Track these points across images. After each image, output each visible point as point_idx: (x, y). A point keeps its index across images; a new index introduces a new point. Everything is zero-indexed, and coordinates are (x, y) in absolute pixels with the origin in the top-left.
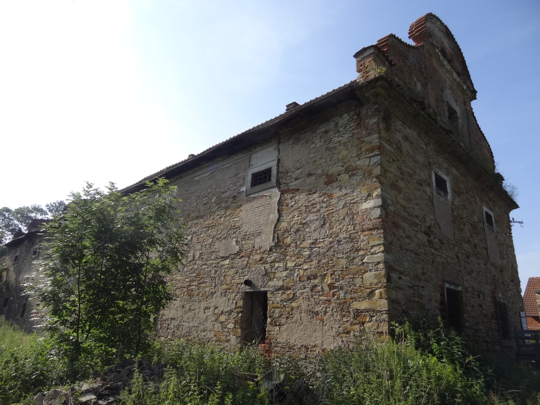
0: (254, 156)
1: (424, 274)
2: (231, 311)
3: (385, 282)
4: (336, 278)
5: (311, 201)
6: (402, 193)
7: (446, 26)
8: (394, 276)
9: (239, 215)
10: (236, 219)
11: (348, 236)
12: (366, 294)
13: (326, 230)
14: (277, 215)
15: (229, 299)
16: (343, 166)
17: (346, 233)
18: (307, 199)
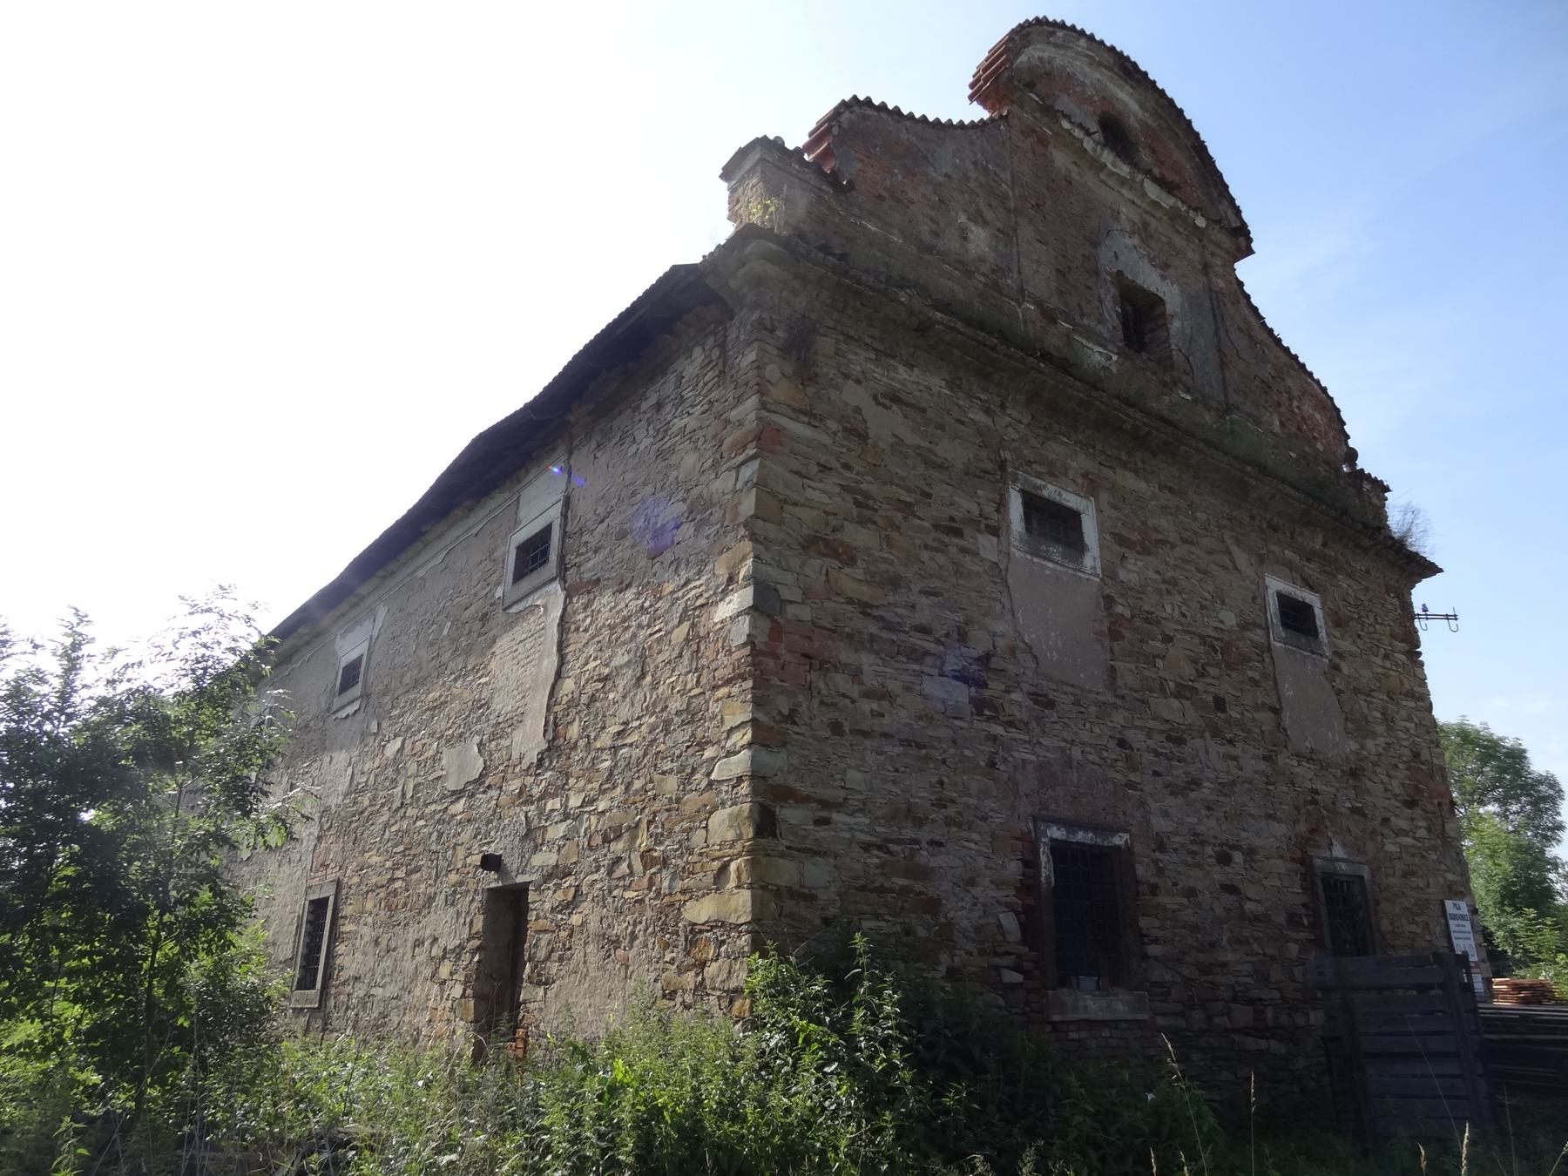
0: (526, 494)
1: (941, 804)
2: (461, 947)
3: (751, 835)
4: (657, 834)
5: (621, 610)
6: (860, 563)
7: (1113, 49)
8: (790, 815)
9: (489, 669)
10: (483, 680)
11: (685, 706)
12: (710, 879)
13: (643, 695)
14: (555, 659)
15: (458, 914)
16: (684, 500)
17: (681, 696)
18: (615, 607)
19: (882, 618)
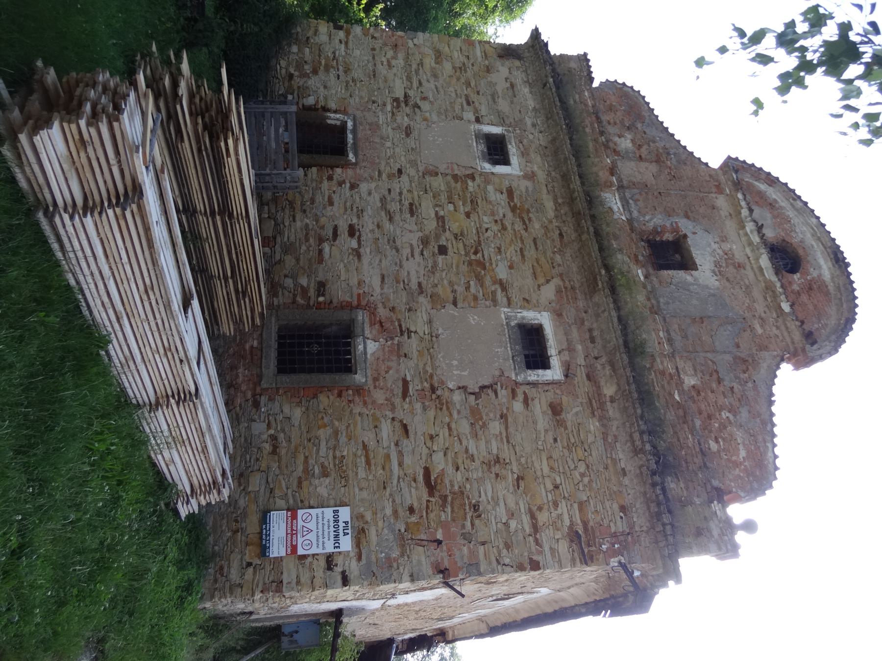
1: (354, 80)
19: (419, 69)
